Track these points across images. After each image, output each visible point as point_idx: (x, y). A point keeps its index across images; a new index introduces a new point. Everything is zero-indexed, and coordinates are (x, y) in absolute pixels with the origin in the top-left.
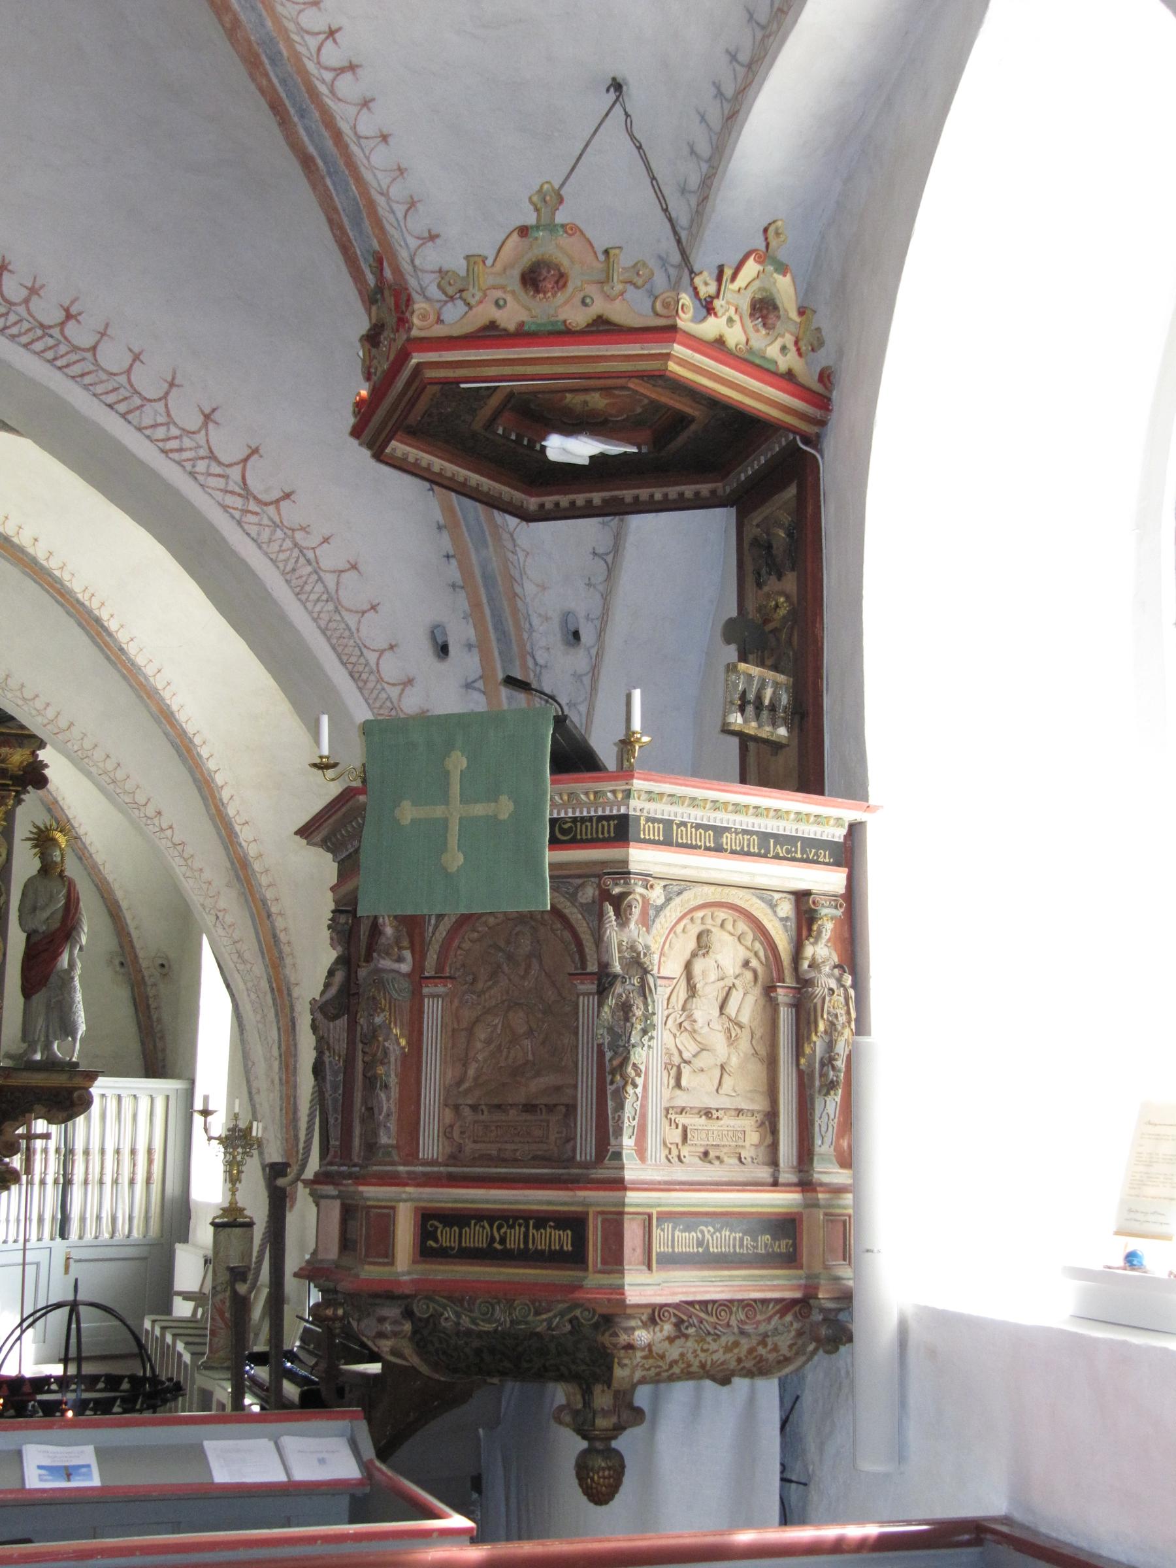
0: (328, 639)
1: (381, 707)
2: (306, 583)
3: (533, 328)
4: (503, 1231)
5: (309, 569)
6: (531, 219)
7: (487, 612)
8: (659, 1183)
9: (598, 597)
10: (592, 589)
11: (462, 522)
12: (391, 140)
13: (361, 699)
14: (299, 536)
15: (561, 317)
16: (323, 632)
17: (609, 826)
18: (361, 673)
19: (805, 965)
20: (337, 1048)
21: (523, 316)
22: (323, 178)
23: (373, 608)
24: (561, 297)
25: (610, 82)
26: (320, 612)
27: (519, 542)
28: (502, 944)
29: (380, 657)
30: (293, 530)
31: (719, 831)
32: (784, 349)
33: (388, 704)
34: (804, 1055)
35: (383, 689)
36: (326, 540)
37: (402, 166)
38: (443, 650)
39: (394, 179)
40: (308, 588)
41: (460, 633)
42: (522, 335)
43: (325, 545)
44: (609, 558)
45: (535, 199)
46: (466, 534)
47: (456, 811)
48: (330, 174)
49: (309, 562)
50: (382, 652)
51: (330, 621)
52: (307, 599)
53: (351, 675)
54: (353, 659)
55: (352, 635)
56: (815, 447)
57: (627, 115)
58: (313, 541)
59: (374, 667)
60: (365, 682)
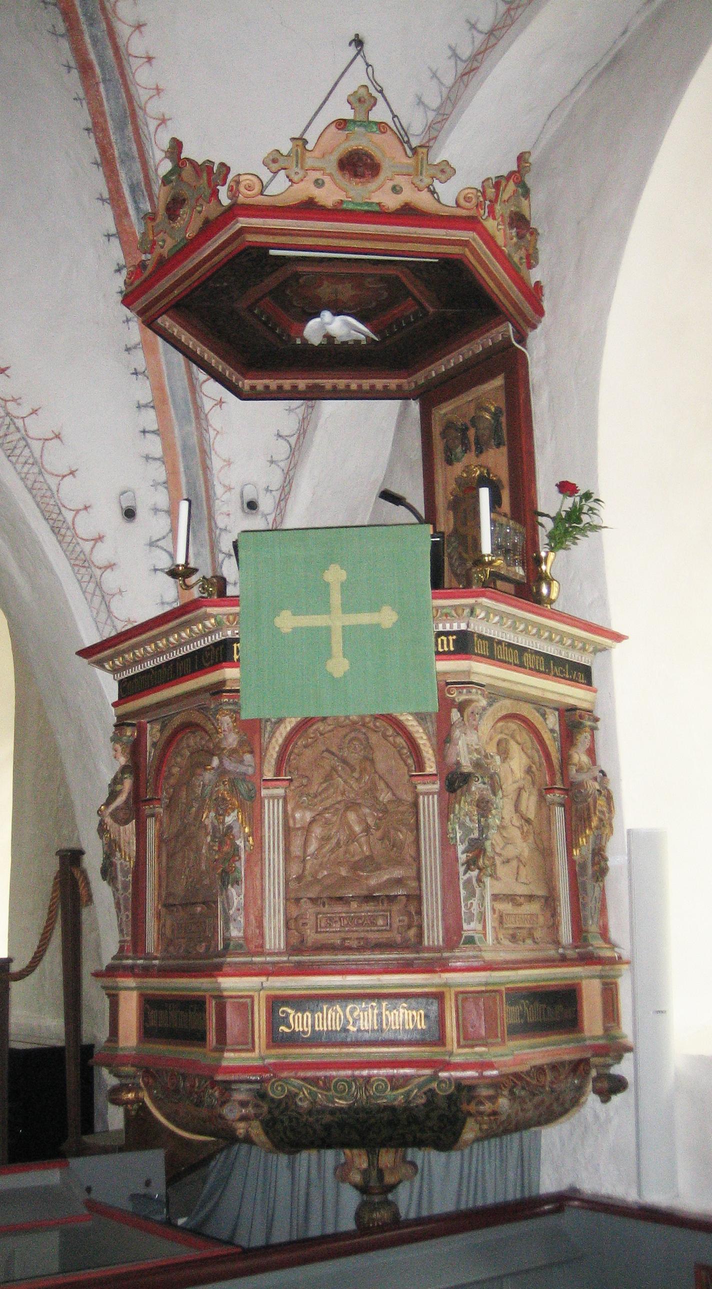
0: (34, 497)
1: (76, 559)
2: (15, 447)
3: (351, 207)
4: (356, 1014)
5: (18, 436)
6: (349, 114)
7: (183, 479)
8: (507, 962)
9: (279, 471)
10: (273, 465)
11: (170, 400)
12: (154, 62)
13: (60, 549)
14: (11, 406)
15: (375, 200)
16: (30, 490)
17: (448, 641)
18: (60, 528)
19: (573, 770)
20: (127, 850)
21: (341, 196)
22: (97, 83)
23: (72, 473)
24: (373, 186)
25: (353, 37)
26: (27, 473)
27: (211, 422)
28: (334, 749)
29: (75, 516)
30: (6, 401)
31: (522, 650)
32: (521, 258)
33: (82, 556)
34: (577, 846)
35: (78, 544)
36: (34, 412)
37: (160, 87)
38: (130, 514)
39: (151, 97)
40: (17, 452)
41: (151, 498)
42: (337, 213)
43: (34, 416)
44: (293, 440)
45: (351, 99)
46: (172, 412)
47: (337, 621)
48: (104, 81)
49: (18, 429)
50: (78, 511)
51: (35, 482)
52: (17, 461)
53: (52, 528)
54: (54, 516)
55: (52, 496)
56: (524, 346)
57: (368, 65)
58: (25, 410)
59: (70, 524)
60: (64, 536)
